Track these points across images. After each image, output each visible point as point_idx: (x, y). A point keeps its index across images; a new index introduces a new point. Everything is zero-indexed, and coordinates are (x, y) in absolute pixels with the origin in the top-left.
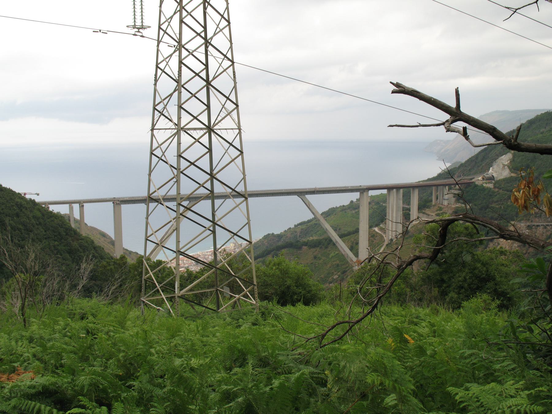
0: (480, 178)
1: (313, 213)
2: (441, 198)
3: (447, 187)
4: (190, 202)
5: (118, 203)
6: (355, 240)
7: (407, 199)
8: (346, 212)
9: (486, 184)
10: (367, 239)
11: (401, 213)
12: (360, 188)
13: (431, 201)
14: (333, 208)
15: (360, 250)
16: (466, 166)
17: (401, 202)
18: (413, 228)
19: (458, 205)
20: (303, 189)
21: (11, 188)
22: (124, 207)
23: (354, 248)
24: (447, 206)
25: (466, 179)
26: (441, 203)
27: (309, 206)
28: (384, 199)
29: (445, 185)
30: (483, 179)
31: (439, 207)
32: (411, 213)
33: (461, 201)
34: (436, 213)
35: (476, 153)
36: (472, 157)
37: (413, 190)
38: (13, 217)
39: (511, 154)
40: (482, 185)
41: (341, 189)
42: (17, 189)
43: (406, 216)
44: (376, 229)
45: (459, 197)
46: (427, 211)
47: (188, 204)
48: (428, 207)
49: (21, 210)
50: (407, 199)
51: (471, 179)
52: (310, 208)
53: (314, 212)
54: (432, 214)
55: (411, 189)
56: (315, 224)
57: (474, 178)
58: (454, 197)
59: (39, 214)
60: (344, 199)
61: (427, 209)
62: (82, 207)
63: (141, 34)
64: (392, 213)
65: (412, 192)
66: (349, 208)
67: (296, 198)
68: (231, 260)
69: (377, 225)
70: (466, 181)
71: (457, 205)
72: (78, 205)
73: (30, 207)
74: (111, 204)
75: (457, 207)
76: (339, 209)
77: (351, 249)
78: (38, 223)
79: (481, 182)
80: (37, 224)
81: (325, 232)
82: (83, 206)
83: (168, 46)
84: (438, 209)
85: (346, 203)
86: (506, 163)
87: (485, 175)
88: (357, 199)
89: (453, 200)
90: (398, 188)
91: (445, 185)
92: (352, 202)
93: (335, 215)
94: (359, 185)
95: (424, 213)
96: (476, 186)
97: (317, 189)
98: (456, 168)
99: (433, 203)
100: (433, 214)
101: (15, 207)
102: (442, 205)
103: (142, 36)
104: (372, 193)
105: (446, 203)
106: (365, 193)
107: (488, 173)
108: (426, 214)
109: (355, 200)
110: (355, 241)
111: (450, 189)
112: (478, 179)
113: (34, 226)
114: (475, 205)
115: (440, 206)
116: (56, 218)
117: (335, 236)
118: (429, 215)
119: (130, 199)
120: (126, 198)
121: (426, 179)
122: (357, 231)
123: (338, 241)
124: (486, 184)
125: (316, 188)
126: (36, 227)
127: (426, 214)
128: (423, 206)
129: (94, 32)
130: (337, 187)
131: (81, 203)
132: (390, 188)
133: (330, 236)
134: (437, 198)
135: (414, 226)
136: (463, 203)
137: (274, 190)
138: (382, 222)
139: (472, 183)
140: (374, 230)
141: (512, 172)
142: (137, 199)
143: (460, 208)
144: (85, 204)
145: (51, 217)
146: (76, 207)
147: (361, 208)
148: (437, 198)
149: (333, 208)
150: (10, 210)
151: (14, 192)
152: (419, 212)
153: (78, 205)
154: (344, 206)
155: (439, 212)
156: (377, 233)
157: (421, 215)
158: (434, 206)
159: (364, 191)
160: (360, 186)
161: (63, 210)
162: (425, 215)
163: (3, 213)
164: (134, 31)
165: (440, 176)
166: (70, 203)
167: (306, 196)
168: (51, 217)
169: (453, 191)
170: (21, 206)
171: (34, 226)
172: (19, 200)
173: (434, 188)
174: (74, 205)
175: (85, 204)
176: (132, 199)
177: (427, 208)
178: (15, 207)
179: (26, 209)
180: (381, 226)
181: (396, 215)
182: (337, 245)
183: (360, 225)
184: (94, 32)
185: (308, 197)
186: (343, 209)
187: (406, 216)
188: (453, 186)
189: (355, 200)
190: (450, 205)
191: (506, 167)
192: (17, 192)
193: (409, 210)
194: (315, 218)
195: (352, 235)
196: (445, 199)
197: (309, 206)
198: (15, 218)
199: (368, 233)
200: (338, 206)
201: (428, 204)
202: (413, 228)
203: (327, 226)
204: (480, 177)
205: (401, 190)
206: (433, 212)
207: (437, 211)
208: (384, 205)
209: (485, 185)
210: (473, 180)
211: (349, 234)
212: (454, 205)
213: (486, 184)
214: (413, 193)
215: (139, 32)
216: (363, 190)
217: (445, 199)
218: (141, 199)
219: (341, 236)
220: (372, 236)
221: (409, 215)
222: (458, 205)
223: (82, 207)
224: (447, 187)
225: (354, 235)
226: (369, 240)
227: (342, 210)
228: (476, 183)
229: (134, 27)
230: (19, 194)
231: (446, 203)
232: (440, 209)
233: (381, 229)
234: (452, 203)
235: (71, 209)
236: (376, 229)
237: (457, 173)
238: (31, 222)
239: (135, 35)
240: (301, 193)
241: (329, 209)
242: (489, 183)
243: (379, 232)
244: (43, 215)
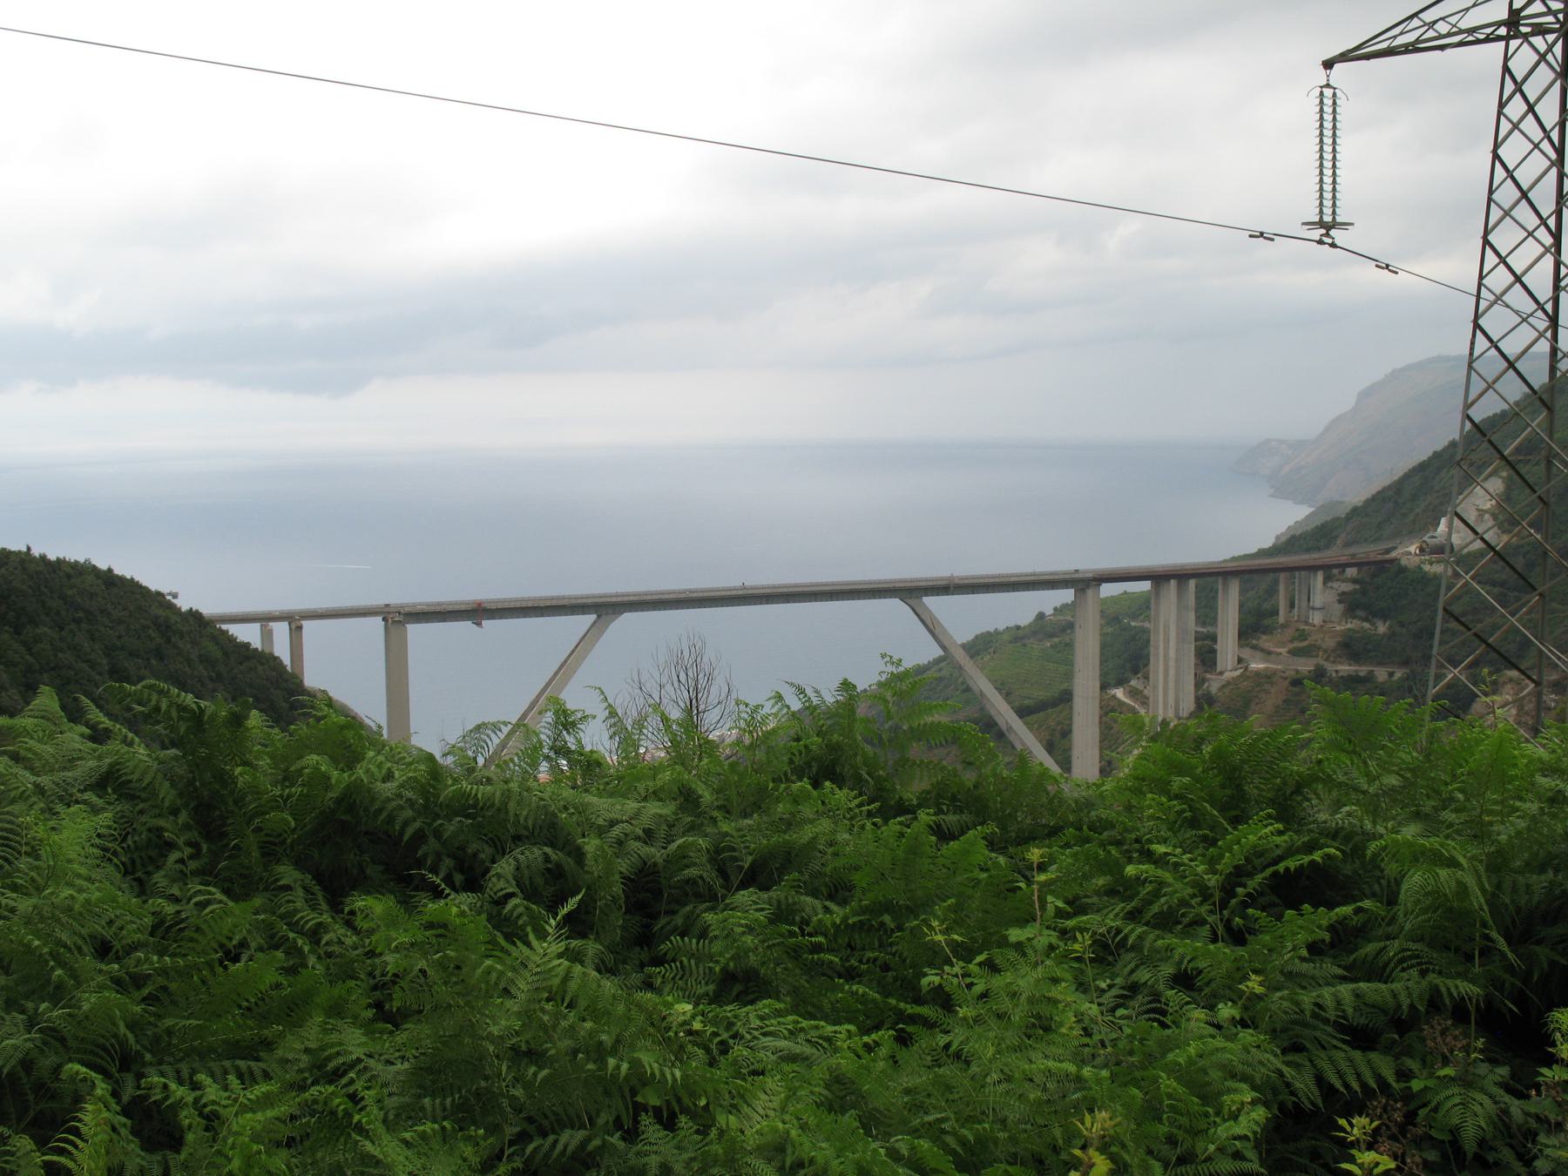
0: (1413, 549)
1: (944, 648)
2: (1304, 604)
3: (1320, 576)
4: (599, 616)
5: (398, 618)
6: (1059, 723)
7: (1207, 611)
8: (1025, 645)
9: (1431, 563)
10: (1097, 719)
11: (1190, 649)
12: (1076, 576)
13: (1277, 613)
14: (988, 633)
15: (1075, 753)
16: (1366, 515)
17: (1192, 616)
18: (1227, 691)
19: (1353, 624)
20: (993, 577)
21: (136, 579)
22: (414, 630)
23: (1058, 744)
24: (1322, 626)
25: (1370, 551)
26: (1303, 619)
27: (931, 626)
28: (1143, 606)
29: (1313, 569)
30: (1422, 550)
31: (1298, 630)
32: (1218, 647)
33: (1360, 613)
34: (1291, 646)
35: (1396, 478)
36: (1384, 490)
37: (1225, 584)
38: (148, 659)
39: (1500, 481)
40: (1419, 567)
41: (1022, 579)
42: (153, 578)
43: (1206, 657)
44: (1119, 693)
45: (1352, 605)
46: (1264, 641)
47: (595, 622)
48: (1268, 631)
49: (169, 641)
50: (1207, 611)
51: (1388, 551)
52: (937, 632)
53: (946, 643)
54: (1279, 650)
55: (1220, 580)
56: (936, 679)
57: (1395, 548)
58: (1340, 602)
59: (214, 651)
60: (1021, 609)
61: (1264, 637)
62: (296, 631)
63: (1330, 241)
64: (1166, 649)
65: (1220, 587)
66: (1035, 633)
67: (895, 605)
68: (1000, 735)
69: (1120, 682)
70: (1372, 557)
71: (1349, 626)
72: (285, 625)
73: (191, 631)
74: (377, 623)
75: (1349, 630)
76: (1006, 637)
77: (1050, 748)
78: (214, 675)
79: (1417, 559)
80: (211, 679)
81: (979, 700)
82: (300, 628)
83: (1377, 266)
84: (1297, 634)
85: (1025, 618)
86: (1488, 506)
87: (1425, 538)
88: (1055, 609)
89: (1338, 609)
90: (1181, 576)
91: (1313, 569)
92: (1041, 616)
93: (994, 652)
94: (1072, 568)
95: (1254, 648)
96: (1403, 570)
97: (956, 581)
98: (1338, 518)
99: (1281, 619)
100: (1283, 650)
101: (151, 631)
102: (1306, 623)
103: (1333, 245)
104: (1108, 590)
105: (1316, 618)
106: (1090, 593)
107: (1436, 534)
108: (1262, 650)
109: (1049, 611)
110: (1059, 728)
111: (1327, 580)
112: (1409, 552)
113: (203, 685)
114: (1402, 625)
115: (1302, 627)
116: (260, 662)
117: (1004, 713)
118: (1269, 653)
119: (432, 609)
120: (420, 604)
121: (1254, 550)
122: (1066, 698)
123: (1015, 727)
124: (1431, 564)
125: (951, 578)
126: (210, 685)
127: (1262, 650)
128: (1253, 627)
129: (1251, 236)
130: (1012, 576)
131: (295, 621)
132: (1159, 578)
133: (993, 712)
134: (1292, 606)
135: (1229, 683)
136: (1366, 620)
137: (594, 596)
138: (1135, 671)
139: (1393, 561)
140: (1114, 697)
141: (1503, 532)
142: (450, 608)
143: (1358, 632)
144: (306, 624)
145: (247, 658)
146: (281, 630)
147: (1079, 636)
148: (1292, 606)
149: (988, 633)
150: (139, 638)
151: (146, 588)
152: (1240, 646)
153: (285, 625)
154: (1018, 628)
155: (1297, 644)
156: (1121, 703)
157: (1246, 653)
158: (1284, 626)
159: (1088, 587)
160: (1077, 571)
161: (248, 634)
162: (1259, 654)
163: (122, 648)
164: (1317, 234)
165: (1291, 543)
166: (264, 619)
167: (925, 599)
168: (247, 658)
169: (1335, 585)
170: (168, 627)
171: (203, 685)
172: (160, 612)
173: (1282, 576)
174: (274, 625)
175: (306, 624)
176: (438, 609)
177: (1264, 633)
178: (151, 631)
179: (182, 637)
180: (1133, 683)
181: (1177, 650)
182: (1012, 738)
183: (1076, 681)
184: (1251, 236)
185: (931, 602)
186: (1018, 635)
187: (1206, 657)
188: (1335, 571)
189: (1049, 611)
190: (1330, 625)
191: (1487, 516)
192: (153, 588)
193: (1214, 639)
194: (946, 658)
195: (1050, 711)
196: (1313, 608)
197: (931, 626)
198: (154, 662)
199: (1097, 705)
200: (1001, 628)
201: (1267, 622)
202: (1227, 691)
203: (983, 684)
204: (1412, 544)
205: (1192, 583)
206: (1282, 644)
207: (1291, 641)
208: (1133, 624)
209: (1427, 568)
210: (1393, 555)
211: (1042, 706)
212: (1339, 624)
213: (1431, 564)
214: (1225, 591)
215: (1327, 235)
216: (1084, 583)
217: (1313, 608)
218: (463, 607)
219: (1022, 712)
220: (1109, 709)
221: (1213, 652)
222: (1353, 624)
223: (296, 631)
224: (1320, 576)
225: (1057, 709)
226: (1100, 723)
227: (1016, 639)
228: (1404, 562)
229: (1321, 224)
230: (159, 594)
231: (1316, 618)
232: (1302, 636)
233: (1134, 693)
234: (1333, 619)
235: (267, 635)
236: (1119, 693)
237: (1343, 535)
238: (196, 673)
239: (1320, 242)
240: (911, 592)
241: (977, 637)
242: (1438, 562)
243: (1127, 701)
244: (226, 654)
